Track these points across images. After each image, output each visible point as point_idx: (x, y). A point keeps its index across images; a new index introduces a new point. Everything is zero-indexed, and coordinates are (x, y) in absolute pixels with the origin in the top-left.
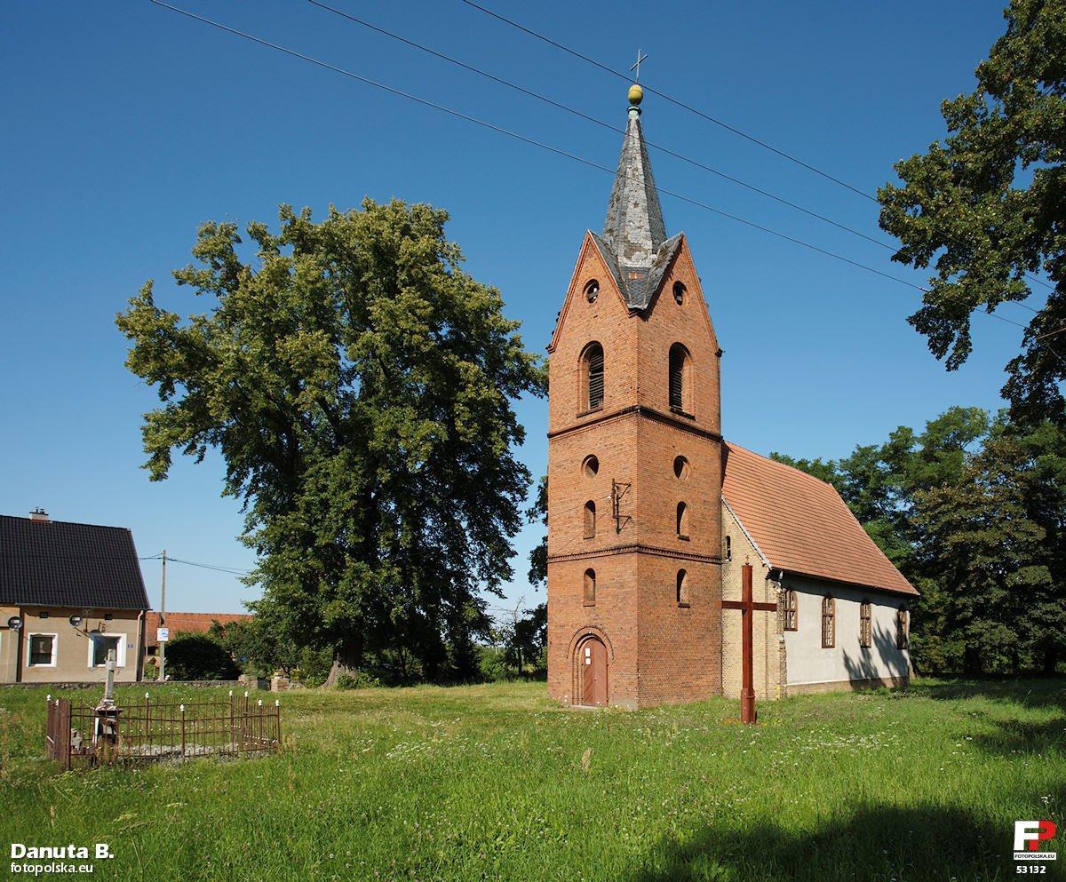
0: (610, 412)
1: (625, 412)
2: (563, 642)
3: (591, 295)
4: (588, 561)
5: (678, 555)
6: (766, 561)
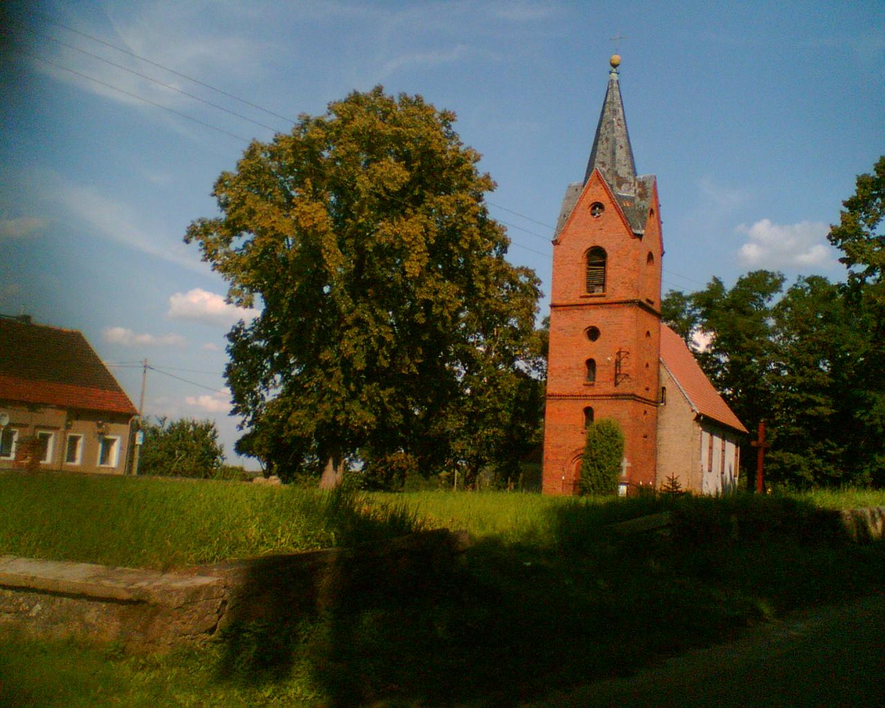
0: (612, 299)
1: (627, 302)
2: (560, 458)
3: (594, 212)
4: (588, 402)
5: (595, 397)
6: (694, 408)
